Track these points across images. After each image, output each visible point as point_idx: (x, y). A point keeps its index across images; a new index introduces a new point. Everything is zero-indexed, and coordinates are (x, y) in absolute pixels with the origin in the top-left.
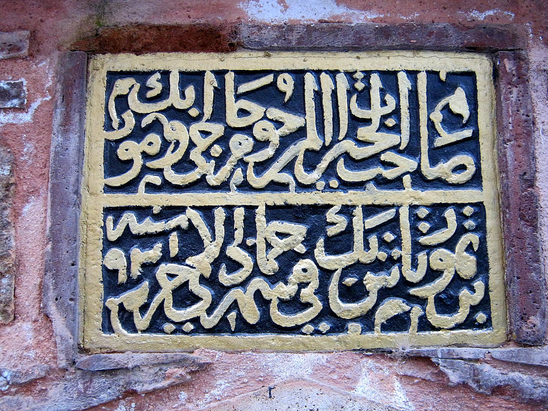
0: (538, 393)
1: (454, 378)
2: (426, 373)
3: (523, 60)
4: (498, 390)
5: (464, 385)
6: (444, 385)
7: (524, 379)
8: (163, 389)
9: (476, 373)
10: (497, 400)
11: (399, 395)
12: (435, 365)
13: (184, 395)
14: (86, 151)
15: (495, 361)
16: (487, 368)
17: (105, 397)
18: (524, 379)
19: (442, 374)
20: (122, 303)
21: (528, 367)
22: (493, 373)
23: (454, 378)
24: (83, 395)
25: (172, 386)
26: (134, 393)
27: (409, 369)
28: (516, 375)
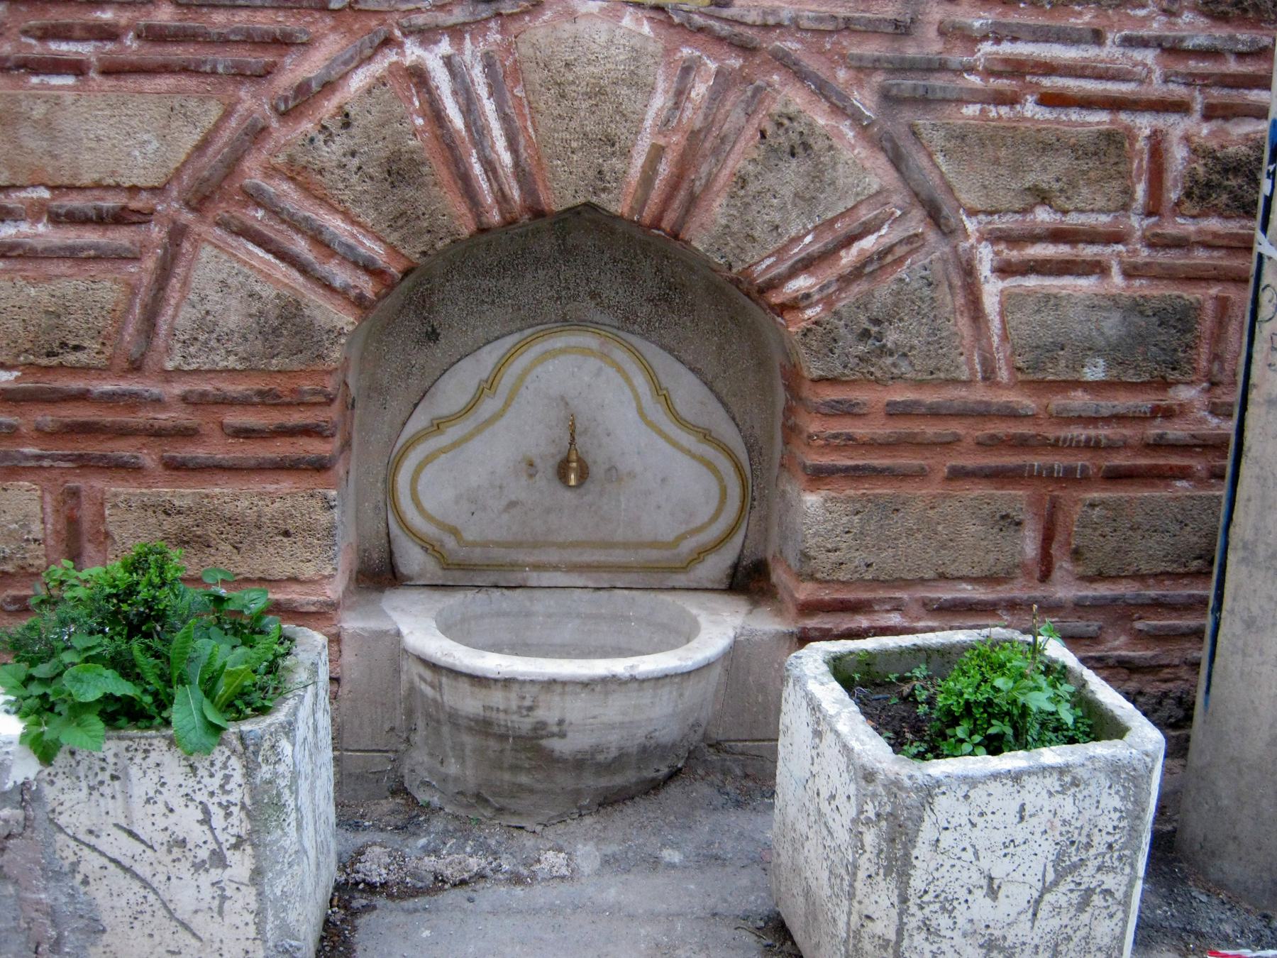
0: (724, 33)
1: (677, 20)
2: (661, 17)
3: (423, 164)
4: (701, 30)
5: (682, 25)
6: (671, 25)
7: (716, 25)
8: (516, 14)
9: (689, 20)
10: (700, 36)
11: (646, 29)
12: (667, 12)
13: (527, 18)
14: (1076, 414)
15: (701, 14)
16: (696, 17)
17: (484, 15)
18: (716, 25)
19: (670, 17)
20: (1269, 89)
21: (719, 18)
22: (699, 20)
23: (677, 20)
24: (472, 14)
25: (522, 13)
26: (500, 15)
27: (652, 14)
28: (712, 22)
